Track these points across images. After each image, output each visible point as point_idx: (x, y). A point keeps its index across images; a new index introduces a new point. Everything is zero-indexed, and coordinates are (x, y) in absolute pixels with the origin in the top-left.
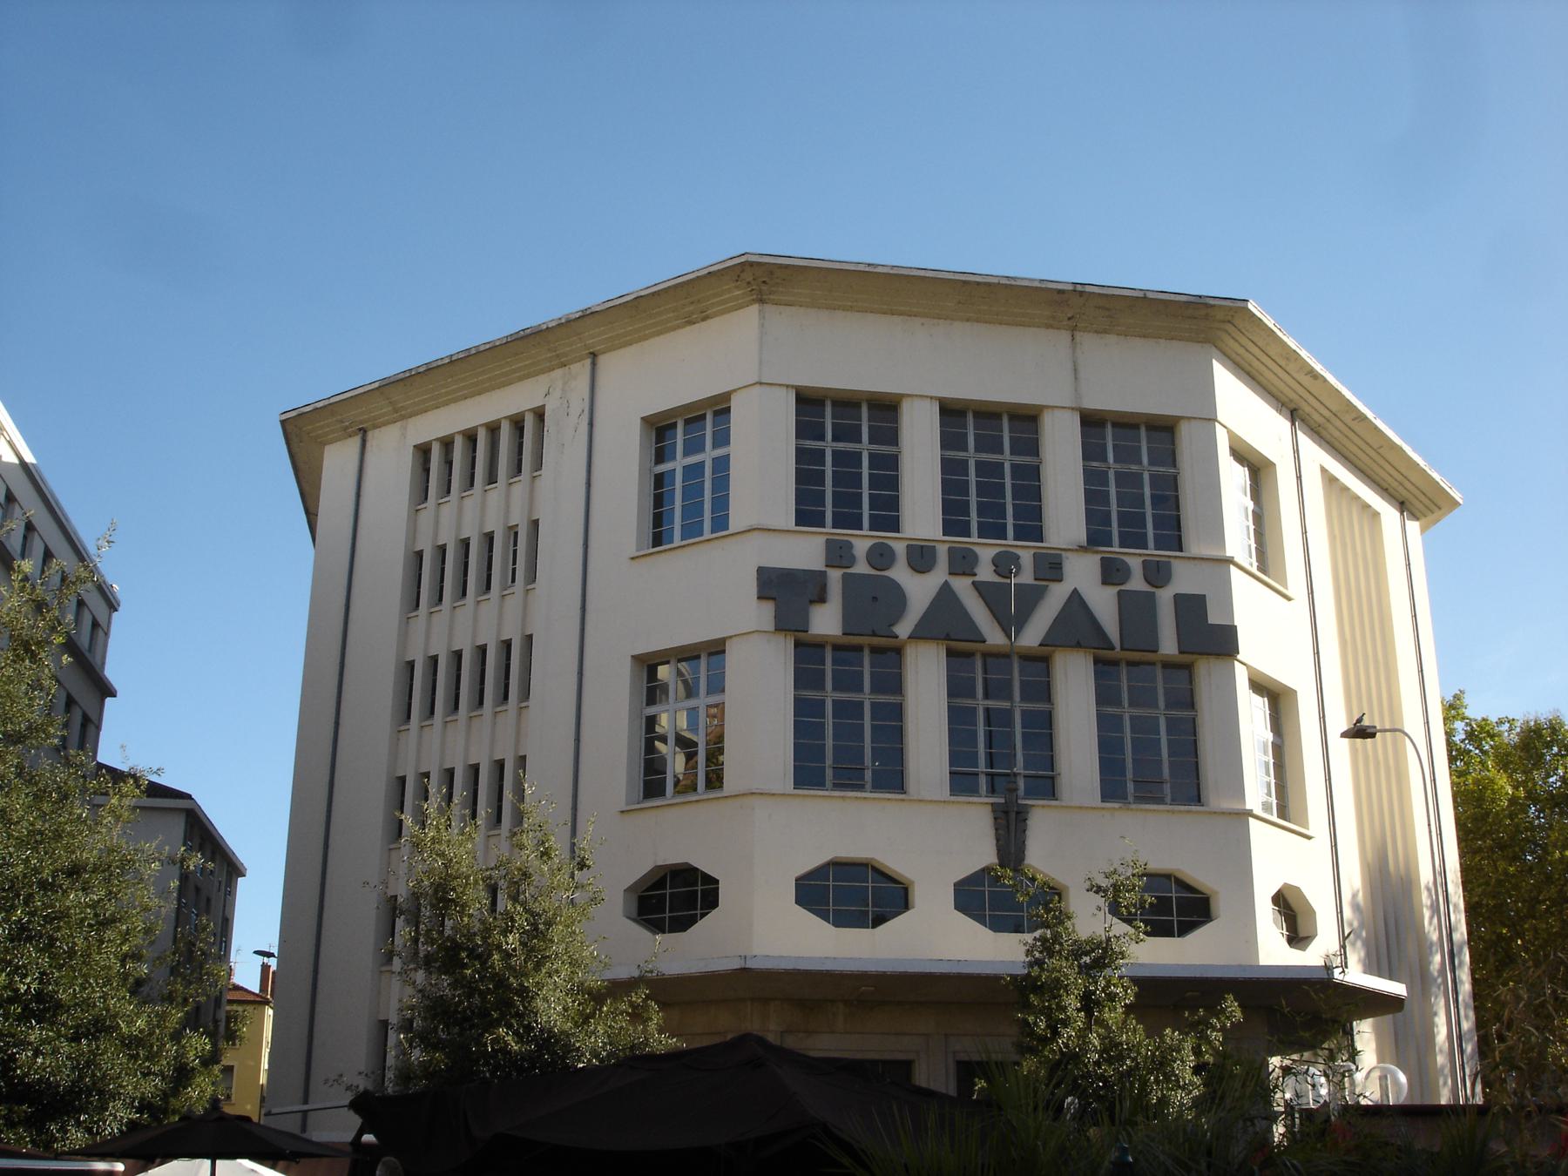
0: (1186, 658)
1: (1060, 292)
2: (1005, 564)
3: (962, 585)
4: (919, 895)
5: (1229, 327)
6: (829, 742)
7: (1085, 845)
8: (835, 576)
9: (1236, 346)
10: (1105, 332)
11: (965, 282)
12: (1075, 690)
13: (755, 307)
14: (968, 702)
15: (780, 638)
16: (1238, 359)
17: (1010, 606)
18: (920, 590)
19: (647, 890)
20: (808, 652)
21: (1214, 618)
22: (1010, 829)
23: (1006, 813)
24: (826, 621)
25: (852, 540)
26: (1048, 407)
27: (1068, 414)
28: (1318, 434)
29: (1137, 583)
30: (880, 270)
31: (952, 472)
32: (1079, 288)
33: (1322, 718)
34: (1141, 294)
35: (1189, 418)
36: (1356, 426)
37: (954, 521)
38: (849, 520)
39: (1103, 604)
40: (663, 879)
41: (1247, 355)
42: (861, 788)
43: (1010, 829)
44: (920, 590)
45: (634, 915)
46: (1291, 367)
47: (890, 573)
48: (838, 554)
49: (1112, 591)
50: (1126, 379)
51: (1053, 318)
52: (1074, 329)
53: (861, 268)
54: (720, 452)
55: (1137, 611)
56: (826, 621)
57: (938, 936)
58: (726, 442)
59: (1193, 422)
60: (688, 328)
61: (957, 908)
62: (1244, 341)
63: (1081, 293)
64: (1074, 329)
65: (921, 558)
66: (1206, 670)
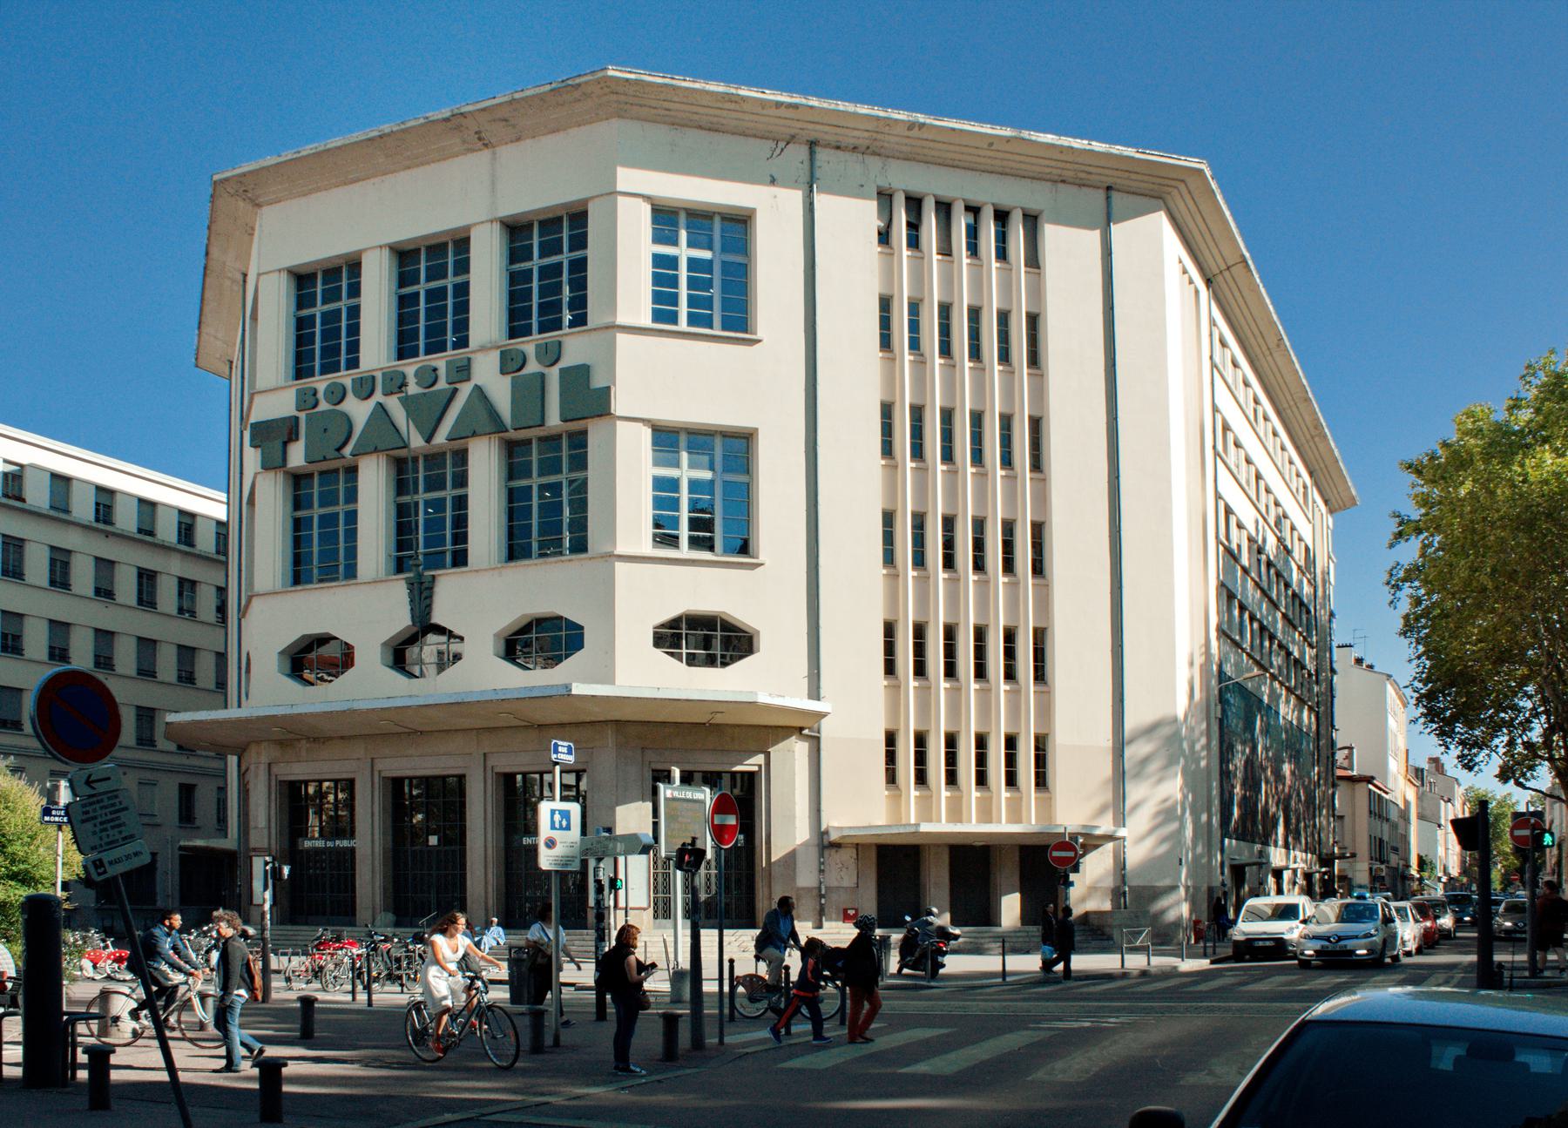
2: (429, 377)
3: (394, 405)
6: (316, 549)
7: (484, 597)
8: (302, 416)
12: (485, 467)
14: (523, 483)
15: (271, 474)
17: (429, 412)
20: (298, 480)
21: (597, 382)
22: (422, 596)
26: (592, 198)
29: (532, 367)
31: (405, 304)
37: (405, 347)
38: (436, 347)
39: (501, 391)
42: (336, 579)
43: (422, 596)
44: (359, 411)
46: (746, 107)
48: (307, 400)
49: (508, 379)
54: (578, 254)
55: (530, 393)
56: (297, 456)
57: (370, 685)
58: (584, 246)
60: (470, 155)
61: (580, 646)
65: (365, 388)
66: (596, 432)
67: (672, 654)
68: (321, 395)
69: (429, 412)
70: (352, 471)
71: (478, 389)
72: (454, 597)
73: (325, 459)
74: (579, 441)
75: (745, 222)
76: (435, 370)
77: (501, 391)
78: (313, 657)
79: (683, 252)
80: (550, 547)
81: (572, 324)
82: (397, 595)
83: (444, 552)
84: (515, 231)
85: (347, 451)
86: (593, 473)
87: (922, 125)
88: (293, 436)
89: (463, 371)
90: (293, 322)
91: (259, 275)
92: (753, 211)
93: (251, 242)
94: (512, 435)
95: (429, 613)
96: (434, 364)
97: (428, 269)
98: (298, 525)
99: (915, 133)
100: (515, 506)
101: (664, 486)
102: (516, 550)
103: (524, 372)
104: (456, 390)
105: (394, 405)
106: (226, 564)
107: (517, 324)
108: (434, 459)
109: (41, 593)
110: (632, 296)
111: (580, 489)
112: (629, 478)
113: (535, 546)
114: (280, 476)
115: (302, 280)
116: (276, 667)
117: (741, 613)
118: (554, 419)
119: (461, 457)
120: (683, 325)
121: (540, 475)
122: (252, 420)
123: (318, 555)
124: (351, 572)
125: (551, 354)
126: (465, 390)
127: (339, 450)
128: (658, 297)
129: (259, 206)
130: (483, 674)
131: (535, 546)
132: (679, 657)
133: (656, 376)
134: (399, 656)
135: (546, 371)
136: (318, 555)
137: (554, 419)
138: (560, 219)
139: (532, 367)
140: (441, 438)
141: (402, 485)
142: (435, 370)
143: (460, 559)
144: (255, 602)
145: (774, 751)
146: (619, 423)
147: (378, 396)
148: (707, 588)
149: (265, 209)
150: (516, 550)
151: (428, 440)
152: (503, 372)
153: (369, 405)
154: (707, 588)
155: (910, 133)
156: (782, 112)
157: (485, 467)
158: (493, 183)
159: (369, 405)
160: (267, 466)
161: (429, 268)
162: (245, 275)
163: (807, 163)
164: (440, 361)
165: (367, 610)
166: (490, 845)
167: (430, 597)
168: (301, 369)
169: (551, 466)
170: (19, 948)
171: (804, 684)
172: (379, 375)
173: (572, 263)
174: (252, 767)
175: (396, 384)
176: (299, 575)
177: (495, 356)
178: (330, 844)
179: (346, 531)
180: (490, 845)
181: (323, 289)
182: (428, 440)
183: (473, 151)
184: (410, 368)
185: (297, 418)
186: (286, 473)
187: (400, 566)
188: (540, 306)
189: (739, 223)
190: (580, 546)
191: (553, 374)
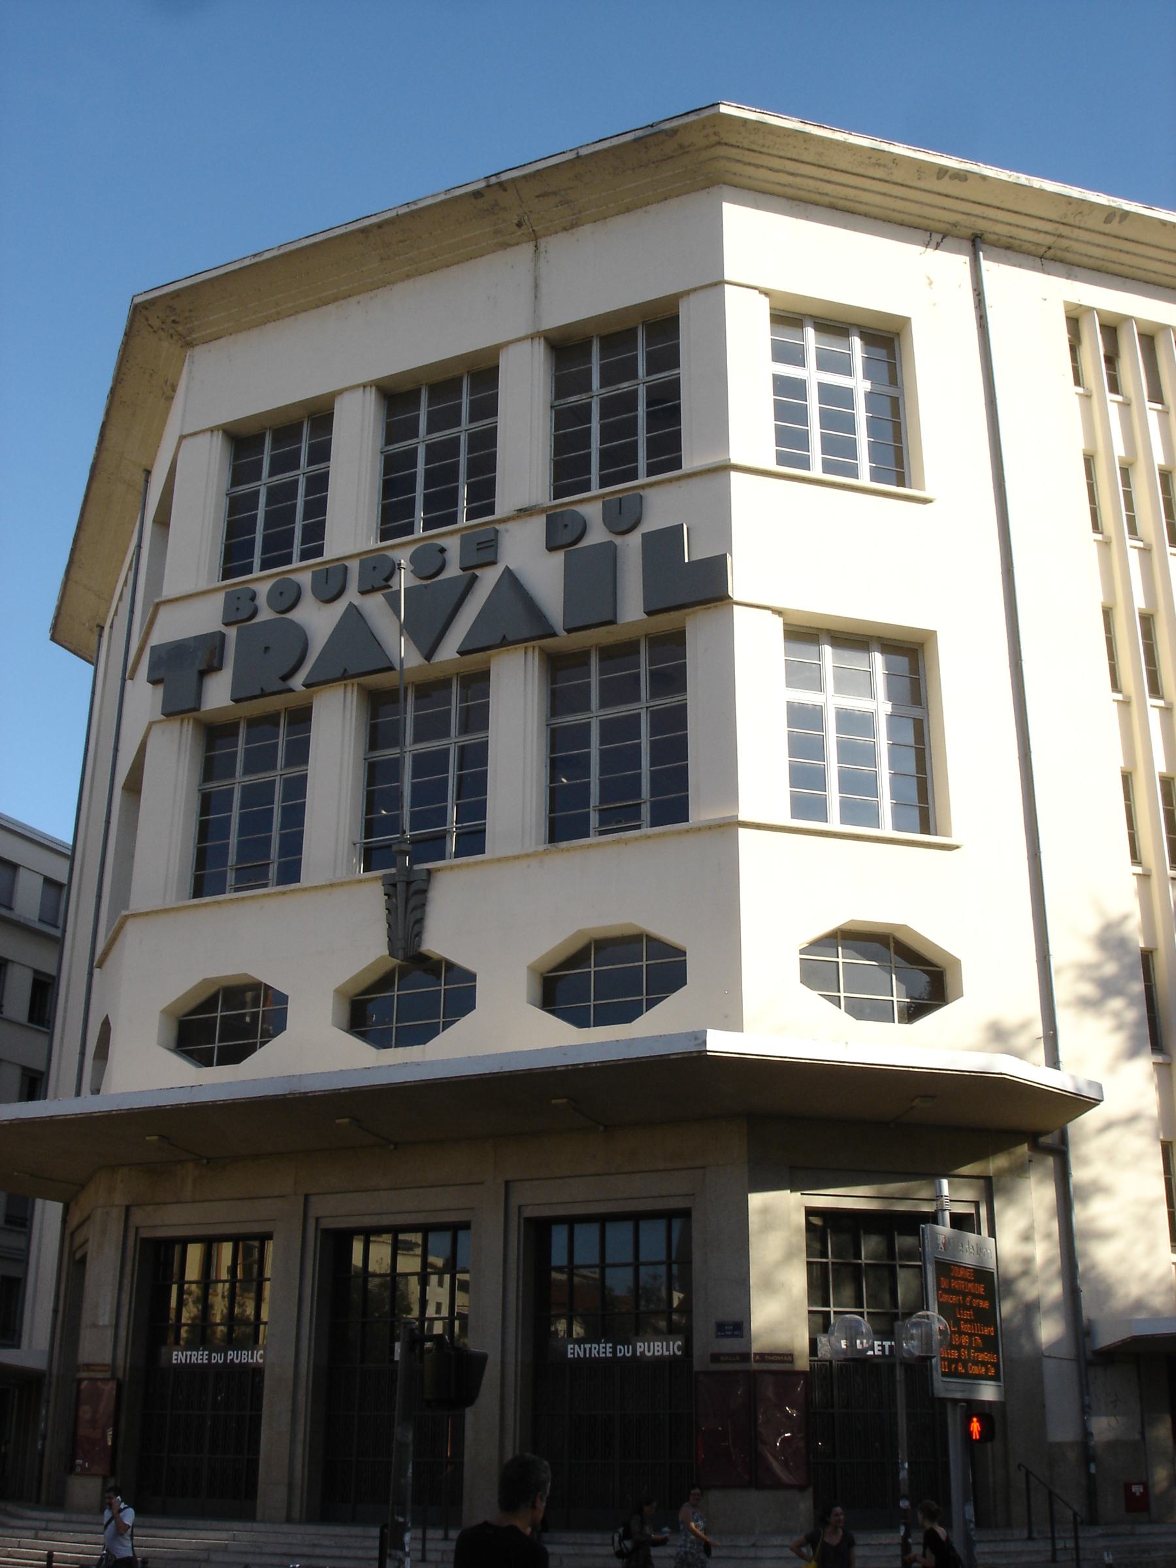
0: (664, 623)
1: (477, 194)
2: (430, 563)
5: (721, 151)
7: (507, 914)
9: (762, 173)
11: (363, 231)
15: (174, 726)
16: (790, 191)
18: (318, 621)
20: (215, 735)
22: (407, 906)
23: (394, 885)
24: (218, 694)
27: (526, 345)
28: (1015, 250)
30: (267, 256)
32: (493, 180)
33: (132, 611)
34: (572, 156)
35: (687, 293)
36: (1114, 227)
37: (394, 519)
39: (544, 575)
41: (798, 181)
43: (407, 906)
44: (318, 621)
45: (173, 1045)
47: (295, 615)
48: (239, 610)
49: (559, 557)
50: (595, 275)
51: (497, 232)
52: (535, 237)
53: (247, 262)
55: (592, 576)
56: (218, 694)
57: (314, 1051)
59: (693, 297)
61: (683, 983)
62: (776, 163)
63: (500, 184)
64: (535, 237)
65: (330, 586)
66: (698, 629)
67: (830, 999)
68: (262, 600)
69: (428, 621)
70: (301, 717)
71: (509, 575)
73: (263, 694)
74: (673, 644)
75: (891, 340)
76: (443, 550)
77: (544, 575)
78: (226, 1020)
79: (812, 376)
80: (620, 816)
81: (652, 470)
83: (442, 837)
84: (566, 349)
85: (297, 682)
86: (696, 697)
87: (1126, 214)
88: (213, 666)
89: (484, 549)
90: (225, 503)
91: (182, 438)
93: (167, 410)
94: (565, 641)
95: (419, 934)
96: (442, 542)
97: (430, 415)
98: (207, 803)
99: (1114, 227)
100: (563, 754)
101: (803, 718)
102: (564, 823)
103: (586, 542)
104: (475, 578)
106: (59, 942)
107: (568, 473)
108: (430, 690)
110: (750, 430)
111: (672, 724)
112: (758, 692)
114: (188, 729)
115: (242, 442)
116: (212, 974)
117: (935, 929)
118: (632, 609)
119: (477, 683)
120: (816, 471)
122: (156, 639)
123: (243, 846)
124: (290, 873)
125: (624, 517)
126: (489, 578)
127: (286, 677)
128: (782, 436)
129: (190, 345)
130: (503, 1030)
132: (836, 1001)
133: (789, 544)
134: (363, 1014)
135: (618, 540)
136: (243, 846)
137: (632, 609)
138: (632, 332)
139: (597, 535)
140: (449, 651)
141: (378, 735)
142: (443, 550)
143: (473, 842)
144: (130, 926)
146: (736, 607)
147: (352, 595)
149: (197, 349)
150: (564, 823)
151: (428, 657)
152: (551, 547)
155: (1107, 228)
156: (946, 186)
158: (536, 286)
160: (171, 712)
161: (438, 413)
162: (148, 473)
165: (311, 941)
166: (510, 1359)
167: (423, 906)
168: (235, 559)
169: (620, 690)
172: (354, 566)
173: (395, 740)
176: (205, 881)
179: (285, 810)
180: (510, 1359)
181: (276, 453)
182: (428, 657)
183: (505, 246)
185: (222, 636)
186: (197, 722)
187: (371, 858)
188: (603, 453)
189: (886, 340)
190: (672, 809)
191: (632, 545)
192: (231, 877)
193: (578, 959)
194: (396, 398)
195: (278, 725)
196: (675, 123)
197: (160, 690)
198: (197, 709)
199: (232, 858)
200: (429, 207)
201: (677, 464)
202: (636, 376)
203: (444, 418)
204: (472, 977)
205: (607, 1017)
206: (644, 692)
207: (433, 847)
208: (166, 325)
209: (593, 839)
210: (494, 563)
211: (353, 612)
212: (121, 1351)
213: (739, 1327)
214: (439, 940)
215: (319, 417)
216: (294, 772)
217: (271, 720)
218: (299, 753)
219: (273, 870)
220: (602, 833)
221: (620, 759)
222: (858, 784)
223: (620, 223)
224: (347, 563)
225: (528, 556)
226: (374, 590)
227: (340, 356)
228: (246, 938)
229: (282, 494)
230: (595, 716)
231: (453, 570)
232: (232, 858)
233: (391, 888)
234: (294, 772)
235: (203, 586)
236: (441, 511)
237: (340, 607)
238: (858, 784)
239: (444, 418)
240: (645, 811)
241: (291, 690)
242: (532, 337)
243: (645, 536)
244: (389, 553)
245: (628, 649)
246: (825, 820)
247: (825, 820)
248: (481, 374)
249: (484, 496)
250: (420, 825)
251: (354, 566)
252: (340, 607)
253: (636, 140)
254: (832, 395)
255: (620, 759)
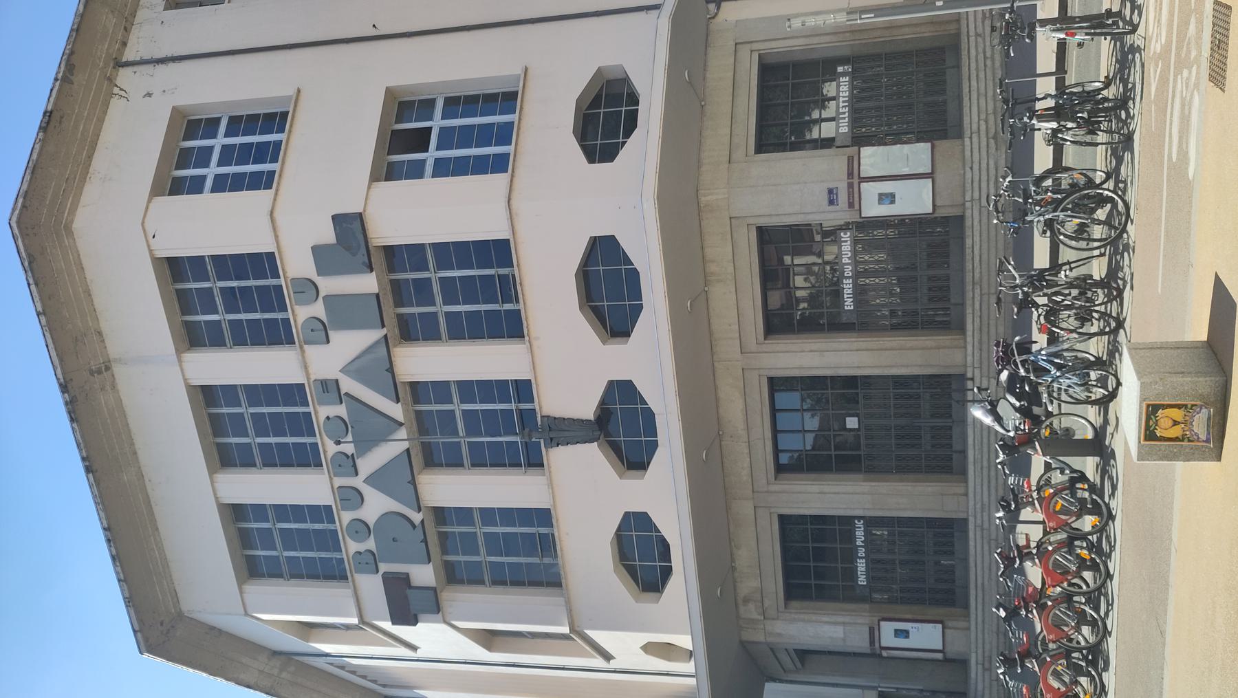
2: (339, 428)
3: (370, 463)
4: (616, 349)
7: (565, 362)
8: (383, 568)
10: (100, 333)
12: (426, 362)
13: (117, 369)
15: (445, 604)
18: (376, 505)
19: (605, 327)
20: (452, 575)
22: (565, 431)
25: (329, 457)
27: (185, 365)
37: (307, 458)
39: (350, 343)
40: (626, 566)
43: (565, 431)
44: (376, 505)
45: (657, 594)
47: (371, 522)
48: (369, 562)
55: (344, 312)
56: (423, 574)
57: (663, 494)
59: (187, 376)
61: (612, 239)
65: (353, 498)
68: (362, 547)
70: (441, 514)
72: (570, 393)
73: (425, 541)
76: (328, 418)
77: (350, 343)
82: (560, 458)
83: (521, 412)
85: (417, 517)
88: (406, 578)
89: (329, 388)
92: (175, 111)
94: (392, 328)
98: (498, 582)
102: (511, 327)
104: (346, 394)
105: (370, 463)
108: (422, 423)
109: (280, 199)
112: (432, 211)
113: (508, 306)
115: (252, 569)
121: (434, 304)
124: (544, 516)
125: (307, 288)
126: (349, 385)
130: (647, 359)
131: (508, 306)
132: (624, 143)
134: (634, 456)
135: (322, 294)
137: (368, 283)
140: (396, 411)
143: (523, 389)
145: (724, 4)
147: (358, 482)
148: (547, 127)
150: (511, 327)
153: (369, 492)
154: (547, 127)
157: (426, 362)
159: (369, 492)
163: (136, 68)
164: (323, 412)
165: (583, 494)
169: (423, 291)
170: (970, 420)
171: (655, 13)
172: (339, 482)
174: (770, 640)
175: (348, 464)
177: (312, 351)
178: (862, 552)
182: (401, 424)
184: (330, 448)
187: (535, 462)
192: (547, 560)
193: (632, 571)
194: (225, 458)
195: (446, 532)
196: (22, 250)
197: (421, 616)
198: (434, 589)
199: (535, 560)
200: (82, 436)
201: (271, 255)
202: (211, 289)
203: (238, 426)
204: (611, 383)
205: (651, 428)
206: (425, 275)
207: (527, 418)
208: (164, 628)
209: (521, 306)
210: (337, 381)
211: (371, 480)
212: (860, 621)
213: (824, 82)
214: (586, 409)
215: (235, 513)
216: (477, 517)
217: (443, 537)
218: (464, 514)
219: (543, 530)
220: (517, 301)
221: (469, 291)
222: (485, 135)
223: (98, 301)
224: (336, 486)
225: (334, 356)
226: (355, 465)
227: (191, 494)
228: (586, 547)
229: (289, 539)
230: (441, 308)
231: (341, 410)
232: (535, 560)
233: (554, 442)
234: (477, 517)
235: (349, 592)
236: (304, 424)
237: (367, 491)
238: (485, 135)
239: (238, 426)
240: (503, 271)
241: (422, 521)
242: (180, 361)
243: (321, 271)
244: (329, 457)
245: (396, 286)
246: (509, 154)
247: (509, 154)
248: (207, 397)
249: (293, 393)
250: (511, 427)
251: (339, 482)
252: (367, 491)
253: (36, 284)
254: (227, 155)
255: (469, 291)
